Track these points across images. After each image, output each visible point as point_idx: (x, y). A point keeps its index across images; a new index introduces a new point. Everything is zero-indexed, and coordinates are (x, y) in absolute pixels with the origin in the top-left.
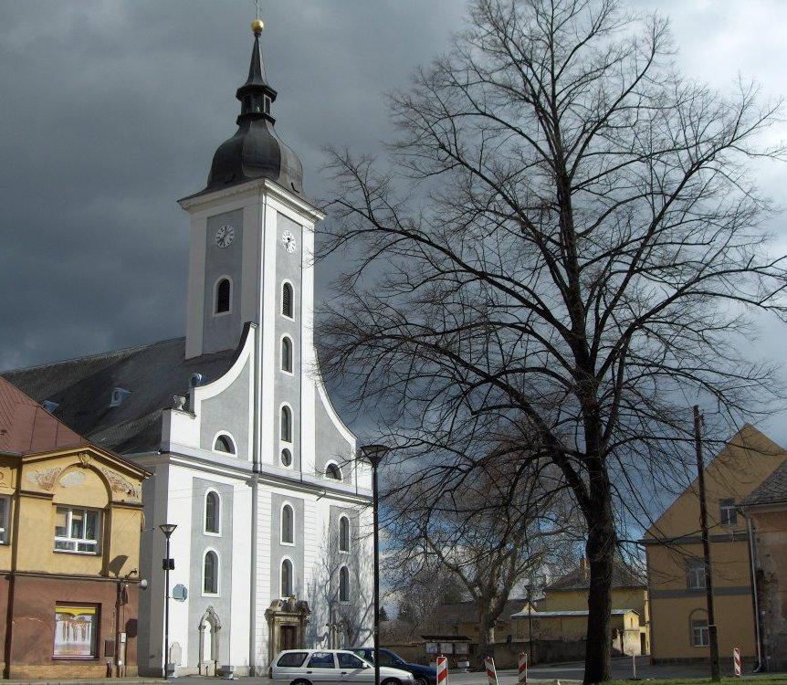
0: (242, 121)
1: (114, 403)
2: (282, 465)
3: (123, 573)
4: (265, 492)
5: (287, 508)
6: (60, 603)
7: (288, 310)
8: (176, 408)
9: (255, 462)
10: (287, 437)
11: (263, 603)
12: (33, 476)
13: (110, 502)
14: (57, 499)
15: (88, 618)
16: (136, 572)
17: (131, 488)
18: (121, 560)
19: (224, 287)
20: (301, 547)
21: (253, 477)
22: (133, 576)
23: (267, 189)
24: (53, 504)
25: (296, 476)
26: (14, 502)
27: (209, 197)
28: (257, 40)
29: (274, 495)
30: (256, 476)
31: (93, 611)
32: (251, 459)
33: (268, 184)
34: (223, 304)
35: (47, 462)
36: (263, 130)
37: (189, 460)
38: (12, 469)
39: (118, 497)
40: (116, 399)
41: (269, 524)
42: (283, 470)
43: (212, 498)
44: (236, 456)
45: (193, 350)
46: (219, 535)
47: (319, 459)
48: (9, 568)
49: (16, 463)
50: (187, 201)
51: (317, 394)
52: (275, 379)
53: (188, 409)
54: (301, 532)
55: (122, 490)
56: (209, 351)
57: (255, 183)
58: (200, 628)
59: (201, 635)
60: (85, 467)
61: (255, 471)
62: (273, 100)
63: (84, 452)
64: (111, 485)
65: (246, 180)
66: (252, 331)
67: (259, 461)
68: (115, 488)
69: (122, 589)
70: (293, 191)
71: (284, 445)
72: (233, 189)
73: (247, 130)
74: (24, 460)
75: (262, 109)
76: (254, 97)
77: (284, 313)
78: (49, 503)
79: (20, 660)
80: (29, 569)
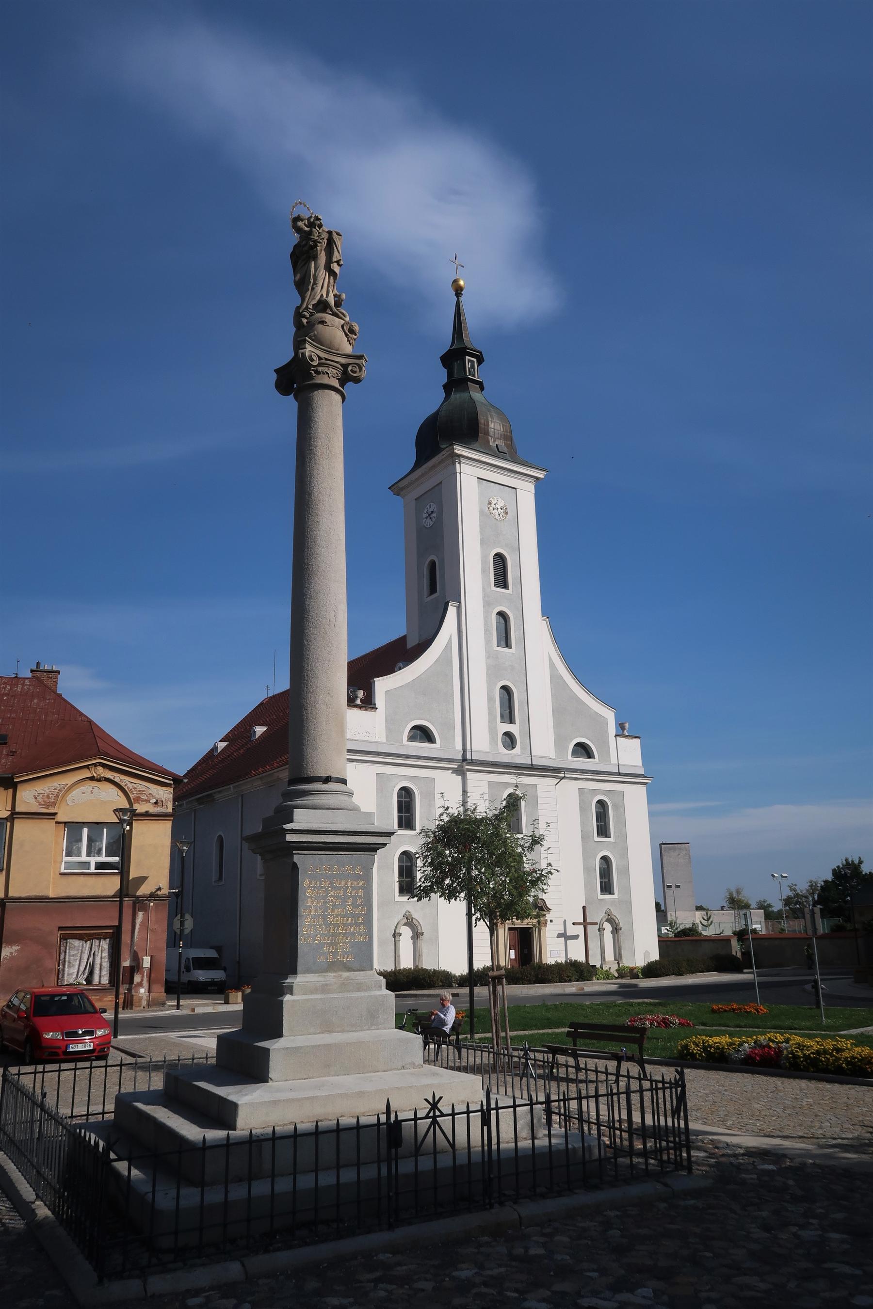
0: (448, 388)
7: (502, 579)
9: (464, 750)
10: (509, 716)
12: (29, 797)
14: (61, 818)
23: (459, 456)
28: (458, 301)
32: (459, 747)
33: (459, 450)
35: (49, 779)
36: (464, 395)
49: (9, 784)
51: (552, 665)
55: (147, 801)
58: (394, 936)
59: (396, 943)
61: (464, 760)
63: (95, 765)
71: (508, 727)
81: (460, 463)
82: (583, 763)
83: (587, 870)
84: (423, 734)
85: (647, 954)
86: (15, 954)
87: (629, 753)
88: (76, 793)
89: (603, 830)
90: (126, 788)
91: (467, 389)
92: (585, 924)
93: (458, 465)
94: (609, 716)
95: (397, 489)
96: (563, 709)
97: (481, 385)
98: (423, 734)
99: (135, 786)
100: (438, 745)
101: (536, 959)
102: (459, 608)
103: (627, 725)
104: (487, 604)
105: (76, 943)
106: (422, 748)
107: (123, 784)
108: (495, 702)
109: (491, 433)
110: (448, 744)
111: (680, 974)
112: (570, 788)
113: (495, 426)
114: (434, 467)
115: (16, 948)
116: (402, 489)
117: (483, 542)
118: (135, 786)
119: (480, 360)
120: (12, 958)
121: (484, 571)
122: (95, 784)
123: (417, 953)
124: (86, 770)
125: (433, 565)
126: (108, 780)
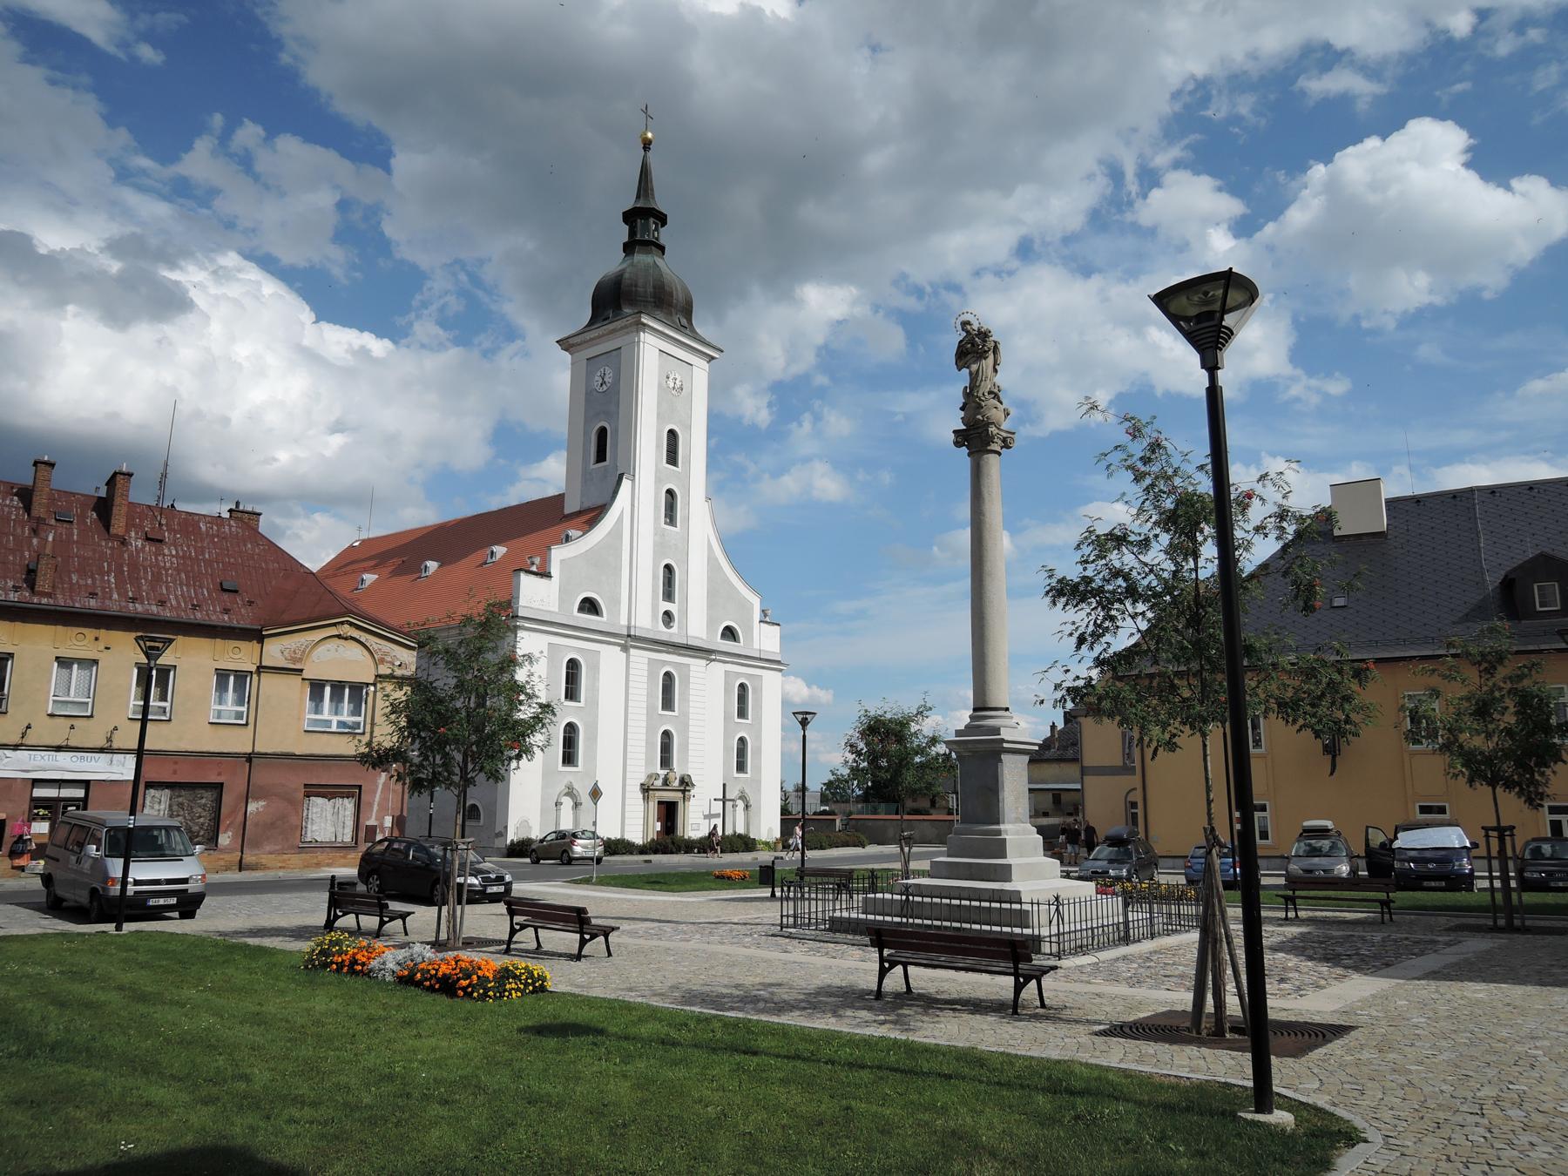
0: (629, 248)
4: (640, 657)
5: (668, 675)
7: (672, 458)
10: (669, 595)
11: (638, 776)
14: (306, 675)
20: (685, 715)
27: (588, 336)
30: (630, 640)
32: (624, 622)
33: (645, 320)
37: (544, 624)
42: (663, 633)
43: (573, 665)
46: (581, 704)
47: (711, 622)
53: (545, 574)
54: (685, 700)
61: (669, 837)
62: (664, 223)
63: (342, 623)
71: (667, 606)
76: (643, 222)
79: (256, 844)
82: (728, 646)
83: (727, 749)
84: (590, 606)
85: (770, 830)
87: (766, 640)
88: (321, 649)
89: (668, 703)
92: (724, 800)
94: (756, 602)
95: (565, 344)
98: (590, 606)
100: (605, 619)
101: (679, 833)
104: (658, 480)
105: (320, 800)
106: (588, 620)
110: (613, 618)
111: (822, 848)
112: (718, 670)
114: (614, 331)
115: (262, 803)
116: (572, 345)
120: (258, 813)
121: (658, 446)
125: (602, 433)
126: (353, 638)
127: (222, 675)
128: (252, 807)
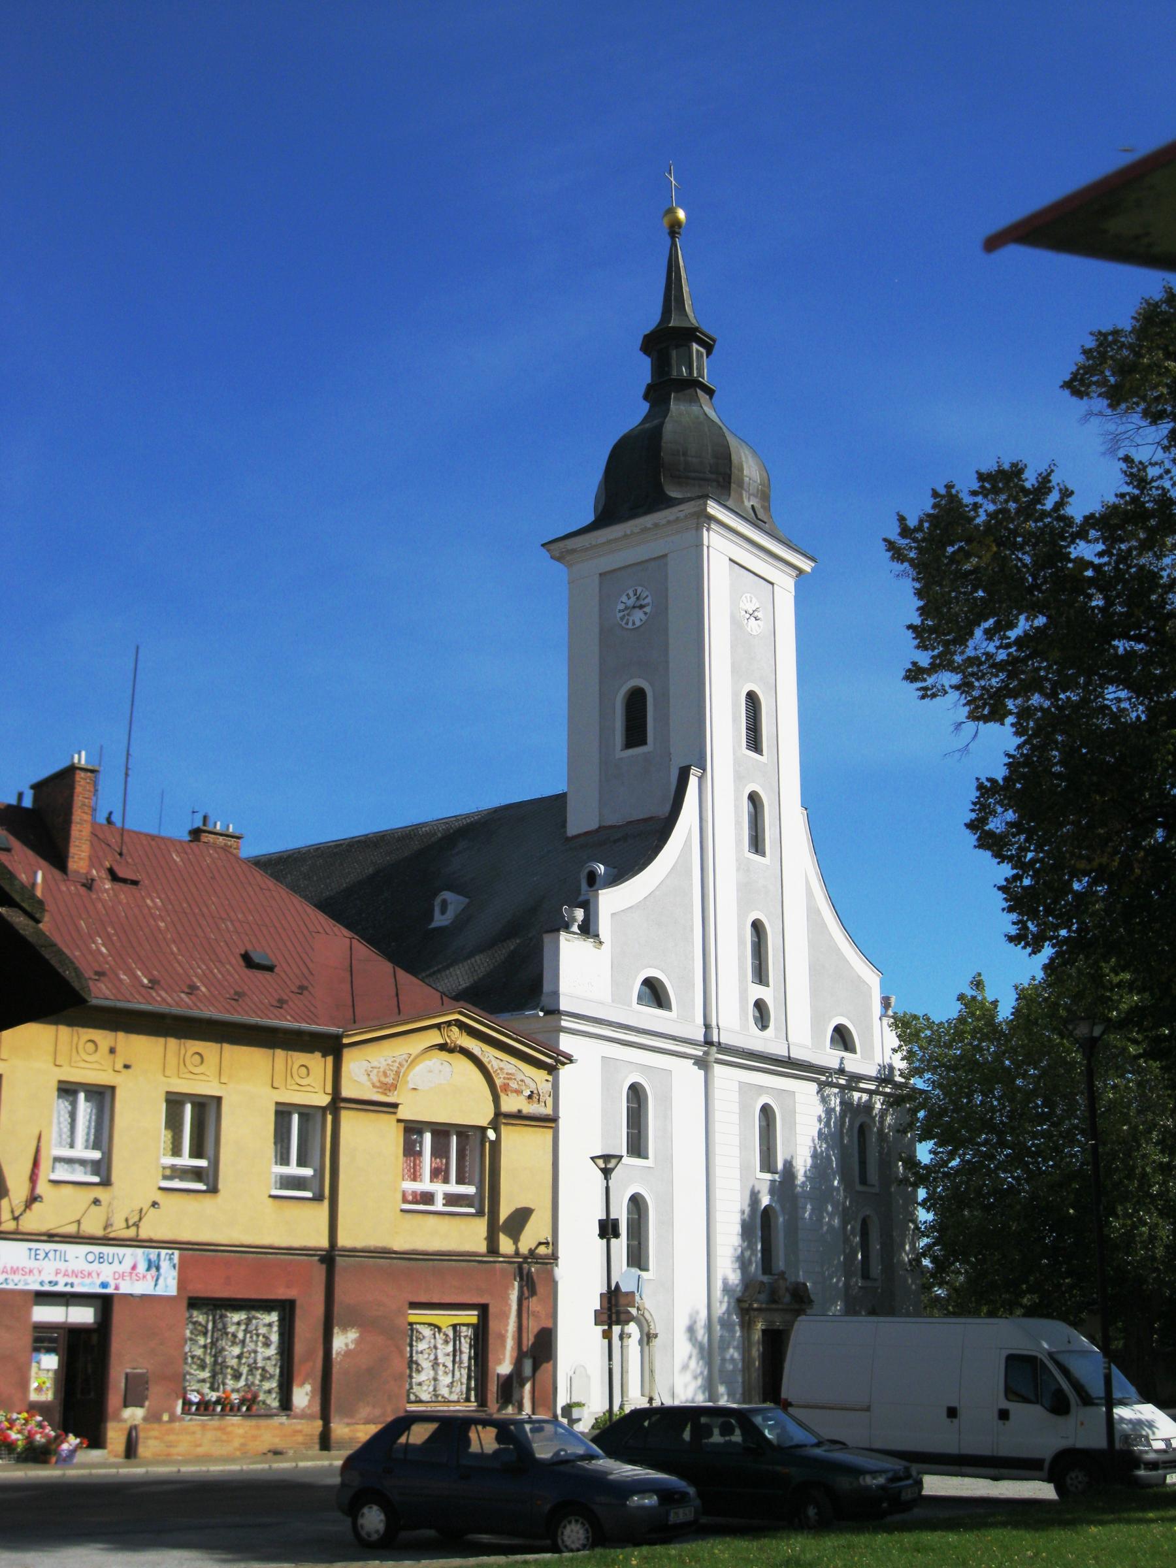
1: (440, 920)
2: (754, 1029)
3: (526, 1243)
4: (727, 1077)
6: (414, 1305)
8: (567, 927)
9: (707, 1026)
10: (761, 976)
12: (361, 1071)
13: (498, 1114)
14: (404, 1113)
15: (466, 1332)
16: (547, 1243)
17: (533, 1087)
18: (522, 1216)
19: (636, 703)
21: (706, 1053)
22: (542, 1250)
23: (711, 518)
24: (399, 1121)
25: (780, 1050)
26: (329, 1118)
29: (743, 1086)
30: (710, 1051)
31: (474, 1320)
33: (713, 508)
34: (635, 733)
36: (695, 409)
38: (324, 1056)
39: (510, 1104)
40: (443, 912)
41: (736, 1141)
42: (757, 1040)
43: (636, 1093)
44: (673, 1015)
45: (580, 821)
47: (817, 1019)
48: (324, 1243)
50: (561, 544)
52: (738, 870)
53: (588, 929)
55: (518, 1092)
56: (613, 819)
57: (689, 508)
60: (451, 1051)
61: (708, 1043)
63: (449, 1023)
64: (498, 1082)
65: (670, 503)
66: (693, 782)
67: (714, 1024)
68: (506, 1088)
69: (525, 1272)
70: (756, 521)
72: (648, 520)
73: (667, 411)
74: (345, 1041)
75: (690, 368)
77: (749, 747)
78: (393, 1118)
80: (359, 1244)
81: (708, 530)
86: (352, 1346)
90: (489, 1067)
91: (695, 400)
93: (705, 533)
94: (872, 980)
95: (560, 547)
96: (822, 969)
97: (710, 392)
99: (502, 1065)
102: (701, 779)
103: (893, 1000)
107: (485, 1060)
108: (745, 947)
109: (745, 486)
113: (750, 468)
117: (735, 669)
118: (502, 1065)
119: (709, 349)
122: (444, 1055)
123: (648, 1372)
124: (435, 1032)
127: (174, 1102)
128: (342, 1341)
